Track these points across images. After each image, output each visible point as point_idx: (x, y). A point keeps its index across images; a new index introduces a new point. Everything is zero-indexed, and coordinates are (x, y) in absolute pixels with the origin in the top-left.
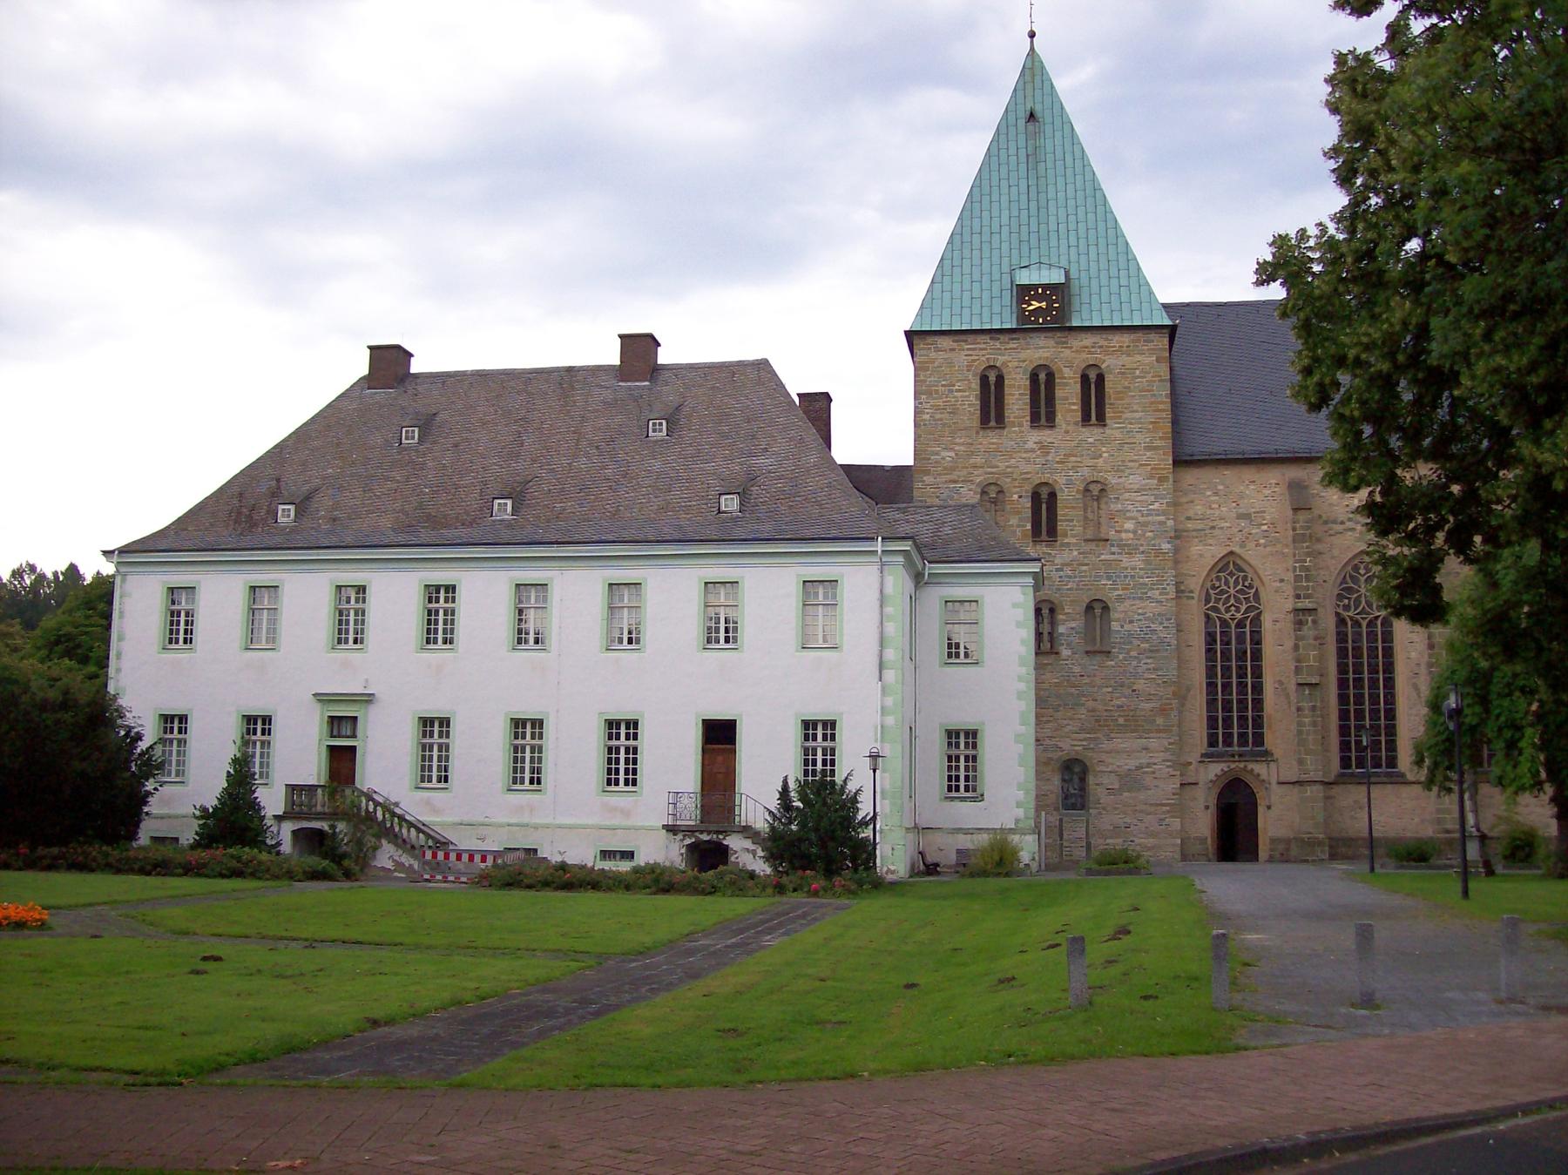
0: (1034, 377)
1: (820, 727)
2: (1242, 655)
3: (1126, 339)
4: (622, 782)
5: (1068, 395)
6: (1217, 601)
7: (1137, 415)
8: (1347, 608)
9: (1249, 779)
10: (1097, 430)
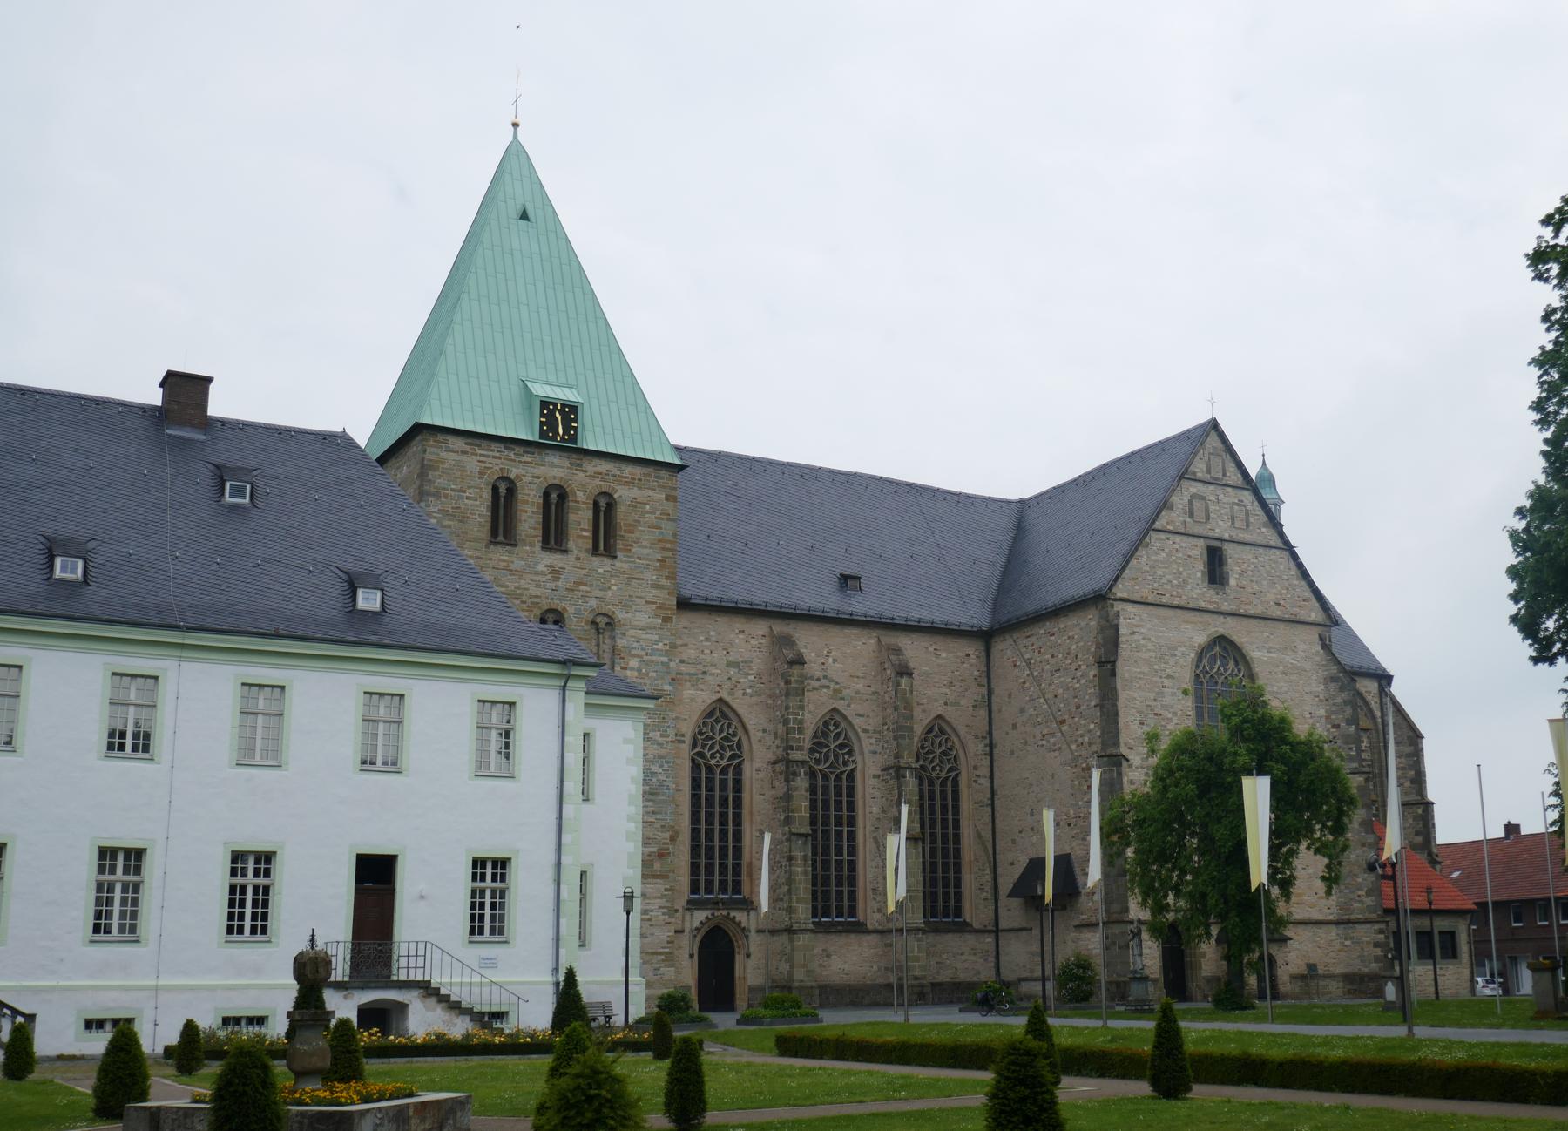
0: (546, 495)
1: (121, 857)
2: (724, 801)
3: (638, 471)
4: (247, 929)
5: (580, 519)
6: (704, 746)
7: (646, 551)
8: (818, 761)
9: (730, 928)
10: (607, 561)
